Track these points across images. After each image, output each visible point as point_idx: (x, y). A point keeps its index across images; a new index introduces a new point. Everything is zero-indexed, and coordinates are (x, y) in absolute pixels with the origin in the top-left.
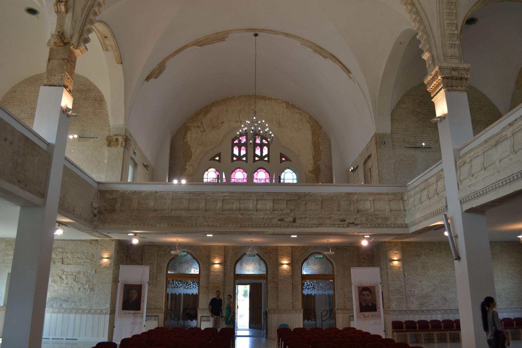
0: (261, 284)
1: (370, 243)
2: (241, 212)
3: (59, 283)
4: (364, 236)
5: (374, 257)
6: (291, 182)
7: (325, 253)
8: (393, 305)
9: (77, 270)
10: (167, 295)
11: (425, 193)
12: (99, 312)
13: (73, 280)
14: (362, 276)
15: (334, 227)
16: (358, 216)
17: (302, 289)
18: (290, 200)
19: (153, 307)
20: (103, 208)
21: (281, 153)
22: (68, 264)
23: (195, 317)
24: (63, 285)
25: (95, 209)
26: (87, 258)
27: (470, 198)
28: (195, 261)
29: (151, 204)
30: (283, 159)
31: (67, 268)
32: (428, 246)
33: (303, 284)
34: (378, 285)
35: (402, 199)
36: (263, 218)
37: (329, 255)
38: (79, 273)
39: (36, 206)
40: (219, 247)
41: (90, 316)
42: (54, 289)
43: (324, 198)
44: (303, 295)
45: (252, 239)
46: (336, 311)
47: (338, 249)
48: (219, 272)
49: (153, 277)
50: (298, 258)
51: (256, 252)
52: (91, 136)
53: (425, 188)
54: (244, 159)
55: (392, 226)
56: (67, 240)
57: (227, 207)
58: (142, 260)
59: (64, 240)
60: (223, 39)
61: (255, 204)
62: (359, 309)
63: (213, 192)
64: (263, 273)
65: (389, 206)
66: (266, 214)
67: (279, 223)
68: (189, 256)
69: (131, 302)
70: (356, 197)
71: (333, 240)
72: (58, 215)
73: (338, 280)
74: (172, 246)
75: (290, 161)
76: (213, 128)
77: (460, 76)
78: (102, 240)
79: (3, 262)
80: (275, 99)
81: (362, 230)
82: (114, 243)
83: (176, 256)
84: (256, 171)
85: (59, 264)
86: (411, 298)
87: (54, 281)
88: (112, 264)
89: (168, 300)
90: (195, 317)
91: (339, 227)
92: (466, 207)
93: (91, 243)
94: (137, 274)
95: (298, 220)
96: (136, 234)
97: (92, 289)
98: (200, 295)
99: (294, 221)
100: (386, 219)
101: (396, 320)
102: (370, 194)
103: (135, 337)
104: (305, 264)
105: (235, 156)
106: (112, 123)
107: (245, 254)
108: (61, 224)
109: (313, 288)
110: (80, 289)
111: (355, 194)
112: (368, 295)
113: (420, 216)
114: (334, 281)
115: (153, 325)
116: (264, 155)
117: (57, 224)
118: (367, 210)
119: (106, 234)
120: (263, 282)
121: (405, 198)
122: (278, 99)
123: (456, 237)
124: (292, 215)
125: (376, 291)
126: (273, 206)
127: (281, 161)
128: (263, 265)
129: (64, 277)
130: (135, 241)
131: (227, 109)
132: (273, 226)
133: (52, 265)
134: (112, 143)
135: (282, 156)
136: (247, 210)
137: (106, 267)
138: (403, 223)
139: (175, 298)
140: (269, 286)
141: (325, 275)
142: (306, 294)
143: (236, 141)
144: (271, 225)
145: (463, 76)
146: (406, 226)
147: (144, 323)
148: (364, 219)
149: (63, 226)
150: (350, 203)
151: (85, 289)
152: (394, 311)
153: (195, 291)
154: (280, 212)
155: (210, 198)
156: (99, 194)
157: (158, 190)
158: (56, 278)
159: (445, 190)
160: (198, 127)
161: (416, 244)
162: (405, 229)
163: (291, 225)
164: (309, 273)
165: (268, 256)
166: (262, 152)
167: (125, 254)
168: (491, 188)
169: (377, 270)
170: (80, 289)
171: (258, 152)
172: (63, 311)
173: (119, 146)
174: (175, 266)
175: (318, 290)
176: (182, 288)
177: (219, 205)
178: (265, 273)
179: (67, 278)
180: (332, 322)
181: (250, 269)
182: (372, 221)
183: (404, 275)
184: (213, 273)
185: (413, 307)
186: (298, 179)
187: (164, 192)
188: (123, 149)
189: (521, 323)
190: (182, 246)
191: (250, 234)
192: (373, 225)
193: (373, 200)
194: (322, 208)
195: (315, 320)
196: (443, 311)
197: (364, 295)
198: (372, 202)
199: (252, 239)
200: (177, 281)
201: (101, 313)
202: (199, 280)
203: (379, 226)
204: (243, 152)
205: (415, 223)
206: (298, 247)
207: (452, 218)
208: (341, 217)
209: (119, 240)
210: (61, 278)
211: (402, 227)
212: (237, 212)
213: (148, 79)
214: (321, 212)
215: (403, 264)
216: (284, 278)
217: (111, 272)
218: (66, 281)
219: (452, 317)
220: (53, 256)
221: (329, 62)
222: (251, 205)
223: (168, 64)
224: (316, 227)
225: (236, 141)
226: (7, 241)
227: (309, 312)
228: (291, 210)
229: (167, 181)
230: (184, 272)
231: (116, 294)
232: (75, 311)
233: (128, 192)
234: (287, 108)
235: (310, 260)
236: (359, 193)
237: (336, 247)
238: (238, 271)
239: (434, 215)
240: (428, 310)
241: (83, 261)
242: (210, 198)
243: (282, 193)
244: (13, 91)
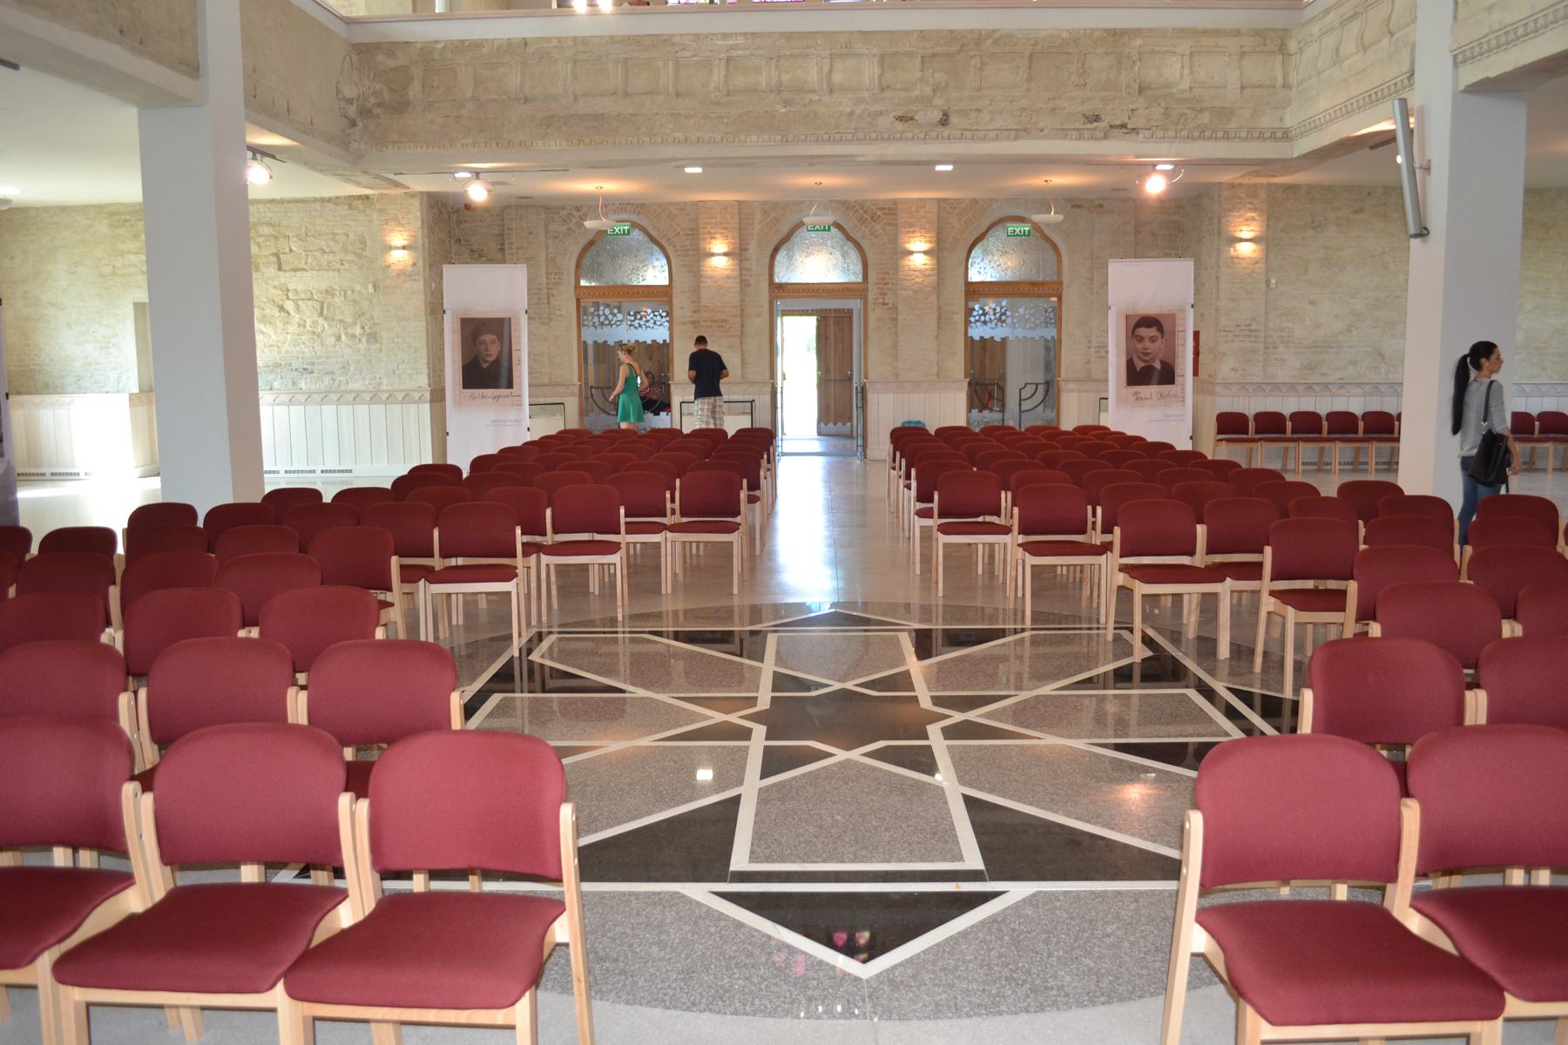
0: (850, 311)
1: (1173, 187)
2: (785, 95)
3: (280, 325)
4: (1154, 165)
5: (1184, 226)
7: (1037, 218)
8: (1226, 369)
9: (324, 286)
10: (583, 346)
11: (1354, 28)
12: (400, 396)
13: (316, 317)
14: (1145, 283)
15: (1065, 137)
16: (1141, 103)
17: (967, 323)
18: (934, 55)
20: (372, 100)
22: (295, 270)
23: (666, 406)
24: (291, 329)
25: (350, 101)
26: (346, 251)
27: (1485, 47)
28: (656, 248)
29: (514, 80)
31: (295, 282)
32: (1356, 191)
33: (969, 311)
34: (1184, 311)
35: (1282, 49)
36: (851, 114)
37: (1048, 225)
38: (329, 292)
39: (178, 101)
40: (724, 206)
41: (378, 409)
42: (272, 341)
43: (1039, 48)
44: (969, 341)
45: (818, 180)
46: (1062, 385)
47: (1079, 206)
48: (728, 277)
49: (540, 297)
50: (959, 233)
51: (829, 219)
53: (1355, 15)
55: (1244, 135)
56: (282, 201)
57: (740, 81)
58: (502, 250)
59: (272, 201)
61: (826, 69)
62: (1124, 377)
63: (697, 37)
64: (853, 279)
65: (1237, 73)
66: (860, 101)
67: (899, 126)
68: (636, 234)
69: (485, 366)
70: (1138, 42)
71: (1061, 180)
72: (248, 125)
73: (1071, 297)
74: (583, 206)
78: (382, 196)
79: (114, 274)
81: (1150, 147)
82: (416, 202)
83: (601, 234)
85: (271, 271)
86: (1281, 349)
87: (264, 320)
88: (420, 264)
89: (586, 361)
90: (666, 406)
91: (1080, 138)
92: (1471, 74)
93: (350, 207)
94: (493, 289)
95: (954, 119)
96: (477, 174)
97: (373, 337)
98: (677, 344)
99: (945, 121)
100: (1225, 113)
101: (1229, 410)
102: (1182, 32)
103: (506, 452)
104: (976, 252)
107: (801, 224)
108: (259, 152)
109: (999, 319)
110: (338, 338)
111: (1136, 32)
112: (1153, 339)
113: (1331, 105)
114: (1060, 299)
115: (549, 426)
117: (249, 154)
118: (1167, 86)
119: (391, 176)
120: (854, 304)
121: (1292, 46)
123: (1427, 169)
124: (938, 101)
125: (1178, 328)
126: (880, 76)
128: (854, 256)
129: (289, 306)
130: (478, 194)
132: (881, 139)
133: (255, 275)
137: (402, 274)
138: (1277, 124)
139: (604, 353)
140: (872, 317)
141: (1034, 284)
142: (977, 338)
144: (874, 135)
146: (1286, 136)
147: (527, 422)
148: (1157, 113)
149: (266, 159)
150: (1119, 62)
151: (353, 336)
152: (1226, 385)
153: (660, 334)
154: (903, 95)
155: (687, 54)
156: (354, 57)
157: (527, 35)
158: (268, 311)
159: (1414, 21)
161: (1311, 191)
162: (1280, 144)
163: (934, 134)
164: (989, 279)
165: (866, 227)
167: (454, 232)
168: (1551, 17)
169: (1185, 267)
170: (338, 338)
172: (302, 398)
174: (599, 264)
175: (1013, 326)
176: (624, 326)
177: (718, 76)
178: (859, 279)
179: (298, 308)
180: (1050, 415)
181: (817, 264)
182: (1178, 116)
183: (1268, 283)
184: (709, 282)
185: (1283, 375)
187: (549, 40)
189: (1559, 426)
190: (613, 205)
191: (813, 163)
192: (1184, 133)
194: (1030, 79)
195: (1003, 411)
196: (1367, 389)
197: (1141, 339)
198: (1186, 59)
199: (818, 180)
200: (607, 306)
201: (407, 399)
202: (670, 303)
203: (1202, 134)
205: (1312, 127)
206: (958, 201)
207: (1421, 109)
208: (1087, 108)
209: (430, 195)
210: (282, 308)
211: (1273, 137)
212: (773, 95)
214: (1028, 90)
215: (1267, 251)
216: (916, 292)
217: (419, 285)
219: (1389, 407)
220: (254, 249)
222: (812, 74)
224: (1008, 138)
226: (112, 214)
227: (984, 391)
228: (936, 89)
229: (554, 5)
230: (626, 281)
231: (442, 349)
232: (334, 397)
233: (440, 46)
235: (991, 241)
236: (1150, 30)
237: (1073, 202)
238: (782, 276)
239: (1373, 99)
240: (1326, 386)
241: (338, 257)
242: (687, 54)
243: (908, 33)
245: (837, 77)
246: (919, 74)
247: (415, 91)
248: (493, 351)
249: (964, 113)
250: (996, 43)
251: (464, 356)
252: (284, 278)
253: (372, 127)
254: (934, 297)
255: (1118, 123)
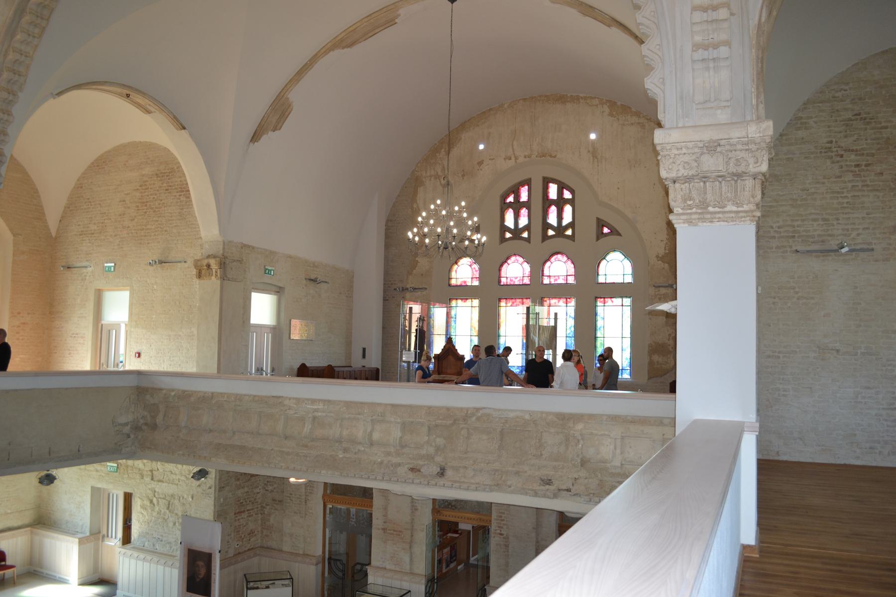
6: (619, 280)
9: (171, 492)
15: (526, 494)
16: (583, 473)
19: (301, 552)
20: (142, 421)
21: (598, 219)
22: (159, 481)
26: (181, 475)
30: (606, 230)
36: (381, 463)
52: (178, 259)
54: (525, 235)
60: (391, 22)
61: (369, 430)
66: (388, 454)
67: (411, 475)
70: (580, 426)
75: (619, 234)
76: (463, 176)
77: (732, 169)
80: (585, 98)
84: (549, 260)
95: (449, 473)
99: (442, 473)
102: (615, 419)
105: (509, 230)
106: (203, 234)
110: (175, 524)
111: (577, 418)
116: (565, 223)
122: (591, 98)
127: (600, 235)
129: (155, 500)
131: (489, 133)
134: (203, 272)
135: (601, 224)
136: (353, 441)
143: (511, 199)
145: (740, 169)
150: (567, 440)
160: (437, 177)
166: (560, 217)
170: (175, 524)
171: (552, 219)
173: (213, 277)
177: (307, 428)
186: (635, 274)
188: (219, 282)
193: (623, 438)
204: (523, 221)
210: (151, 502)
213: (255, 137)
218: (157, 509)
221: (615, 31)
223: (294, 96)
225: (511, 199)
228: (438, 449)
234: (611, 115)
242: (291, 412)
243: (421, 407)
244: (79, 186)
245: (376, 436)
246: (427, 438)
247: (159, 419)
248: (203, 572)
249: (456, 469)
250: (478, 419)
251: (188, 571)
252: (154, 485)
253: (140, 437)
254: (533, 535)
255: (564, 487)
